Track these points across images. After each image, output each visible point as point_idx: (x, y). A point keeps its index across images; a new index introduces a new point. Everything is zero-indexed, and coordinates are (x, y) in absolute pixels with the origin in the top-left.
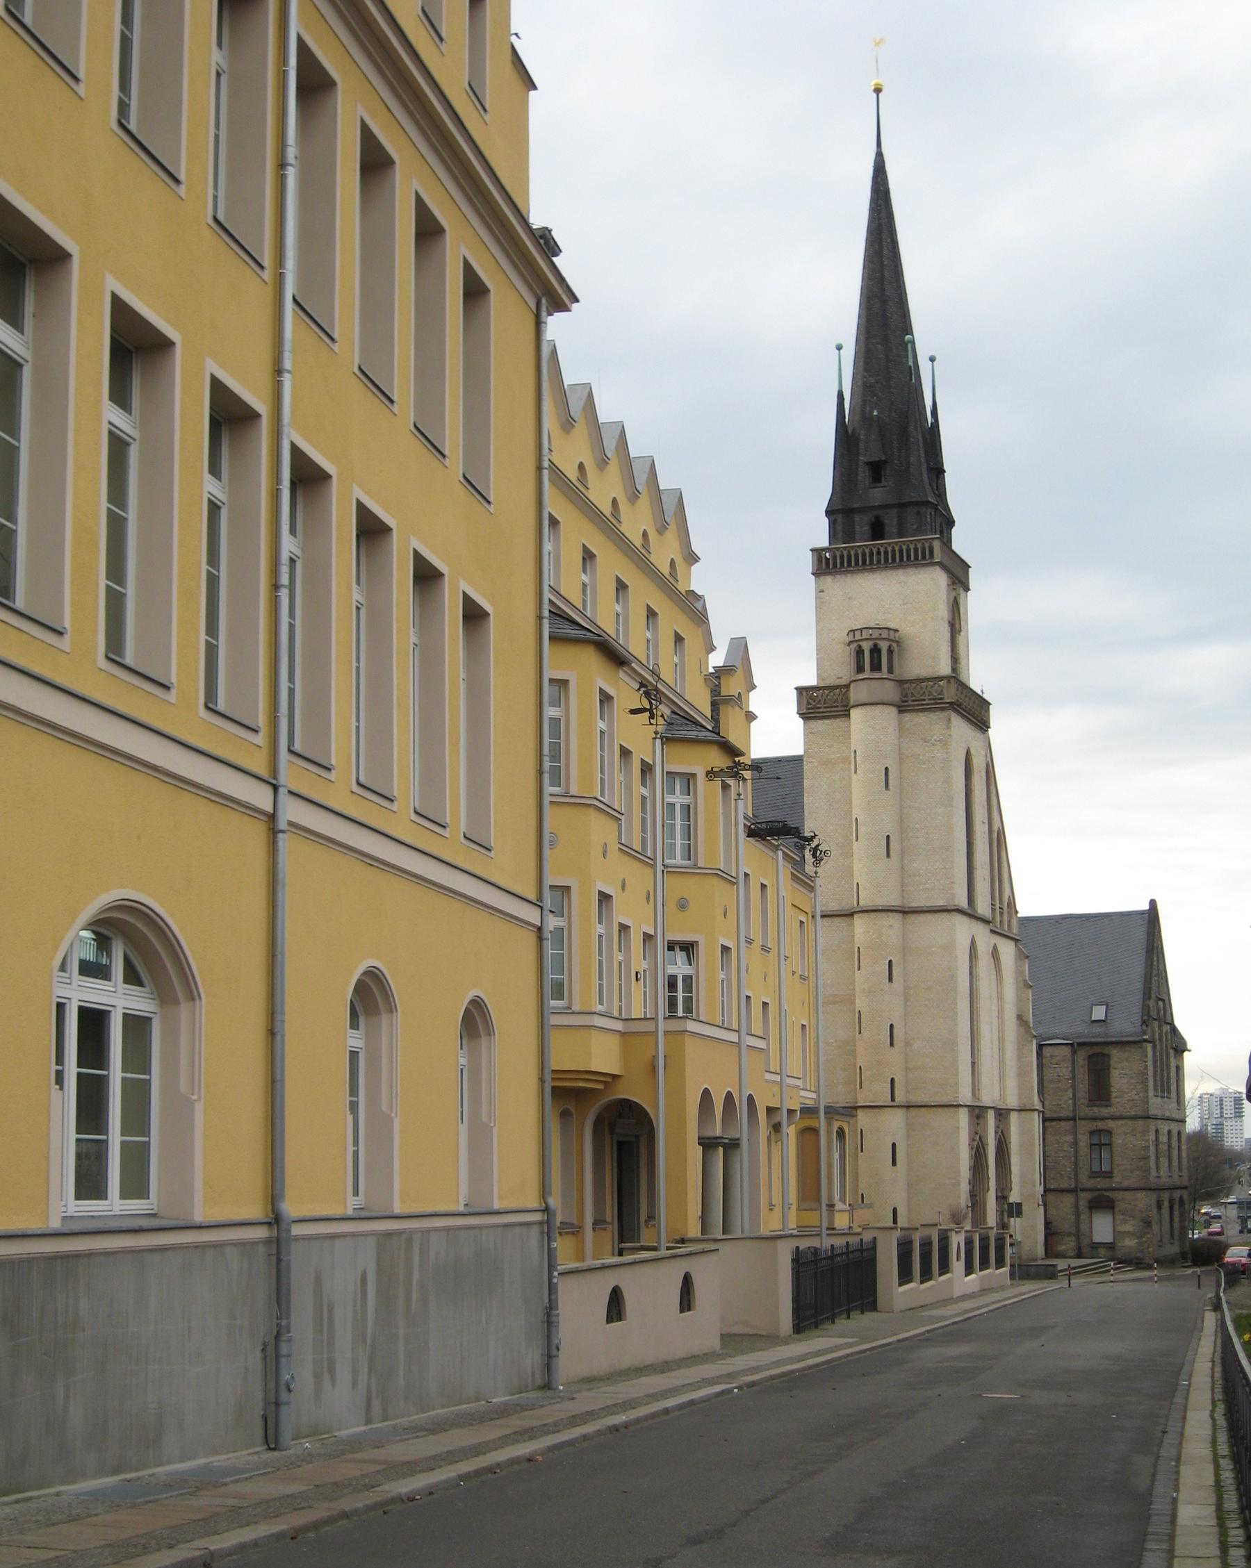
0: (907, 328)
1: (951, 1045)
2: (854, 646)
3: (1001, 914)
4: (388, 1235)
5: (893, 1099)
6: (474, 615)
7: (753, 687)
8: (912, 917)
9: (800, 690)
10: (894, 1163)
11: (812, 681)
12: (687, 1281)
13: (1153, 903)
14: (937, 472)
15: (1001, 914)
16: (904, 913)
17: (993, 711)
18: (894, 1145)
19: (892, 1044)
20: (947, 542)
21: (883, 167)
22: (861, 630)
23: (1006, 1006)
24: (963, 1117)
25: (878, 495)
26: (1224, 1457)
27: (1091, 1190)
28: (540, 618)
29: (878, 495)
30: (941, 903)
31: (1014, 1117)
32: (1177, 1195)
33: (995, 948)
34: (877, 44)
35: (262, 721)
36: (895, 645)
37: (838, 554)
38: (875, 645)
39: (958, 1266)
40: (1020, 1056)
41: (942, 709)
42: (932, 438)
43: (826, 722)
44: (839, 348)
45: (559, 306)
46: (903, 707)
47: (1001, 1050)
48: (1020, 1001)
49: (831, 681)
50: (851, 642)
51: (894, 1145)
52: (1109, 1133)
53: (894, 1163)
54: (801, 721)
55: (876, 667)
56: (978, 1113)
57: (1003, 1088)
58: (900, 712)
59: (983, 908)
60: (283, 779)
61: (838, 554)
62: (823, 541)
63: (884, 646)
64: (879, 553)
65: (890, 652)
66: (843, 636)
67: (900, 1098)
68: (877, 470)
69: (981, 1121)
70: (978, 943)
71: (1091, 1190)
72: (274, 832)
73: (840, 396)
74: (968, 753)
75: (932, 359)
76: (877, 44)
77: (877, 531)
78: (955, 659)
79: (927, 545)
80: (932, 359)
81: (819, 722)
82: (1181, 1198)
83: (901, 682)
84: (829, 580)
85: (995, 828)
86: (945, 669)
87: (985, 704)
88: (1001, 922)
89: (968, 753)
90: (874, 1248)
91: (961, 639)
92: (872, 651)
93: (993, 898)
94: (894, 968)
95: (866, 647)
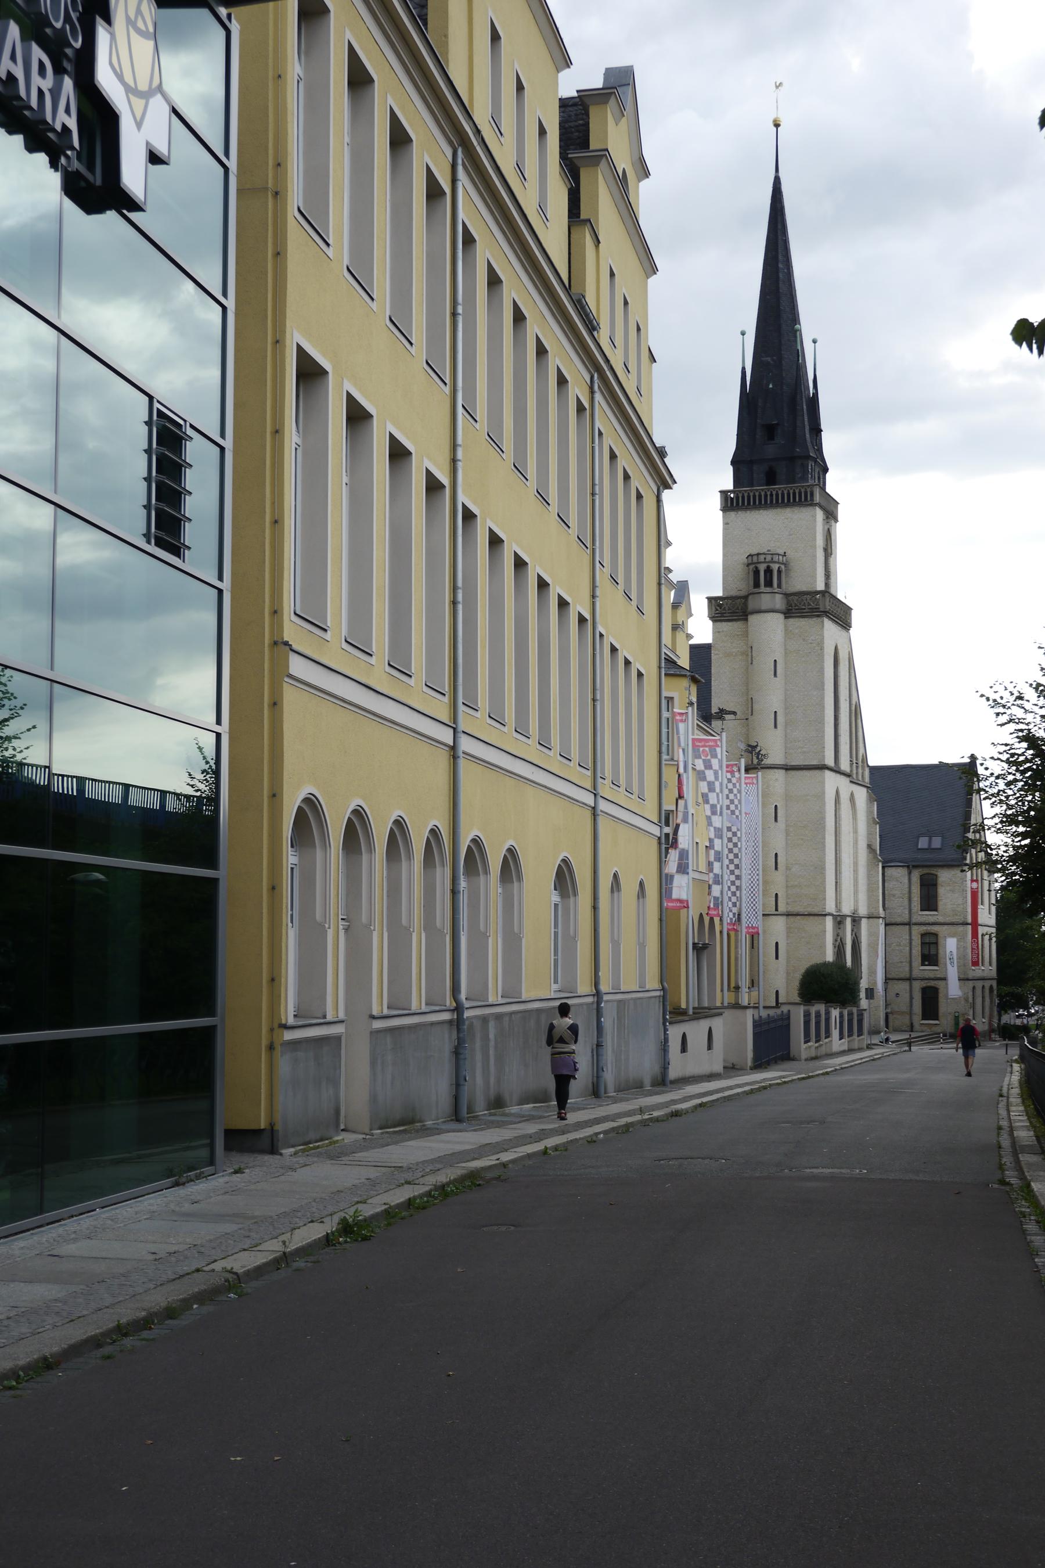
0: (795, 319)
1: (821, 869)
2: (752, 567)
3: (857, 767)
4: (619, 1001)
5: (777, 910)
6: (640, 675)
7: (691, 615)
8: (793, 773)
9: (710, 599)
10: (777, 958)
11: (719, 593)
12: (684, 1036)
13: (973, 758)
14: (817, 431)
15: (857, 767)
16: (786, 769)
17: (853, 613)
18: (777, 943)
19: (776, 868)
20: (823, 488)
21: (780, 189)
22: (758, 554)
23: (860, 838)
24: (829, 922)
25: (771, 450)
26: (1028, 1149)
27: (922, 979)
28: (660, 668)
29: (771, 450)
30: (815, 762)
31: (864, 922)
32: (987, 984)
33: (852, 794)
34: (777, 87)
35: (446, 689)
36: (783, 567)
37: (740, 495)
38: (768, 567)
39: (835, 1033)
40: (870, 876)
41: (818, 616)
42: (813, 403)
43: (730, 624)
44: (743, 334)
45: (668, 487)
46: (788, 613)
47: (856, 871)
48: (870, 834)
49: (734, 593)
50: (748, 565)
51: (777, 943)
52: (936, 935)
53: (777, 958)
54: (710, 623)
55: (769, 583)
56: (839, 921)
57: (856, 901)
58: (786, 618)
59: (845, 766)
60: (462, 727)
61: (740, 495)
62: (729, 485)
63: (775, 567)
64: (772, 495)
65: (779, 571)
66: (743, 558)
67: (782, 908)
68: (770, 431)
69: (841, 926)
70: (841, 792)
71: (922, 979)
72: (455, 757)
73: (744, 369)
74: (836, 648)
75: (815, 341)
76: (777, 87)
77: (771, 478)
78: (828, 575)
79: (809, 490)
80: (815, 341)
81: (724, 624)
82: (991, 987)
83: (787, 595)
84: (732, 514)
85: (854, 703)
86: (820, 586)
87: (848, 610)
88: (857, 773)
89: (836, 648)
90: (789, 1018)
91: (831, 560)
92: (766, 572)
93: (851, 757)
94: (779, 811)
95: (762, 568)
